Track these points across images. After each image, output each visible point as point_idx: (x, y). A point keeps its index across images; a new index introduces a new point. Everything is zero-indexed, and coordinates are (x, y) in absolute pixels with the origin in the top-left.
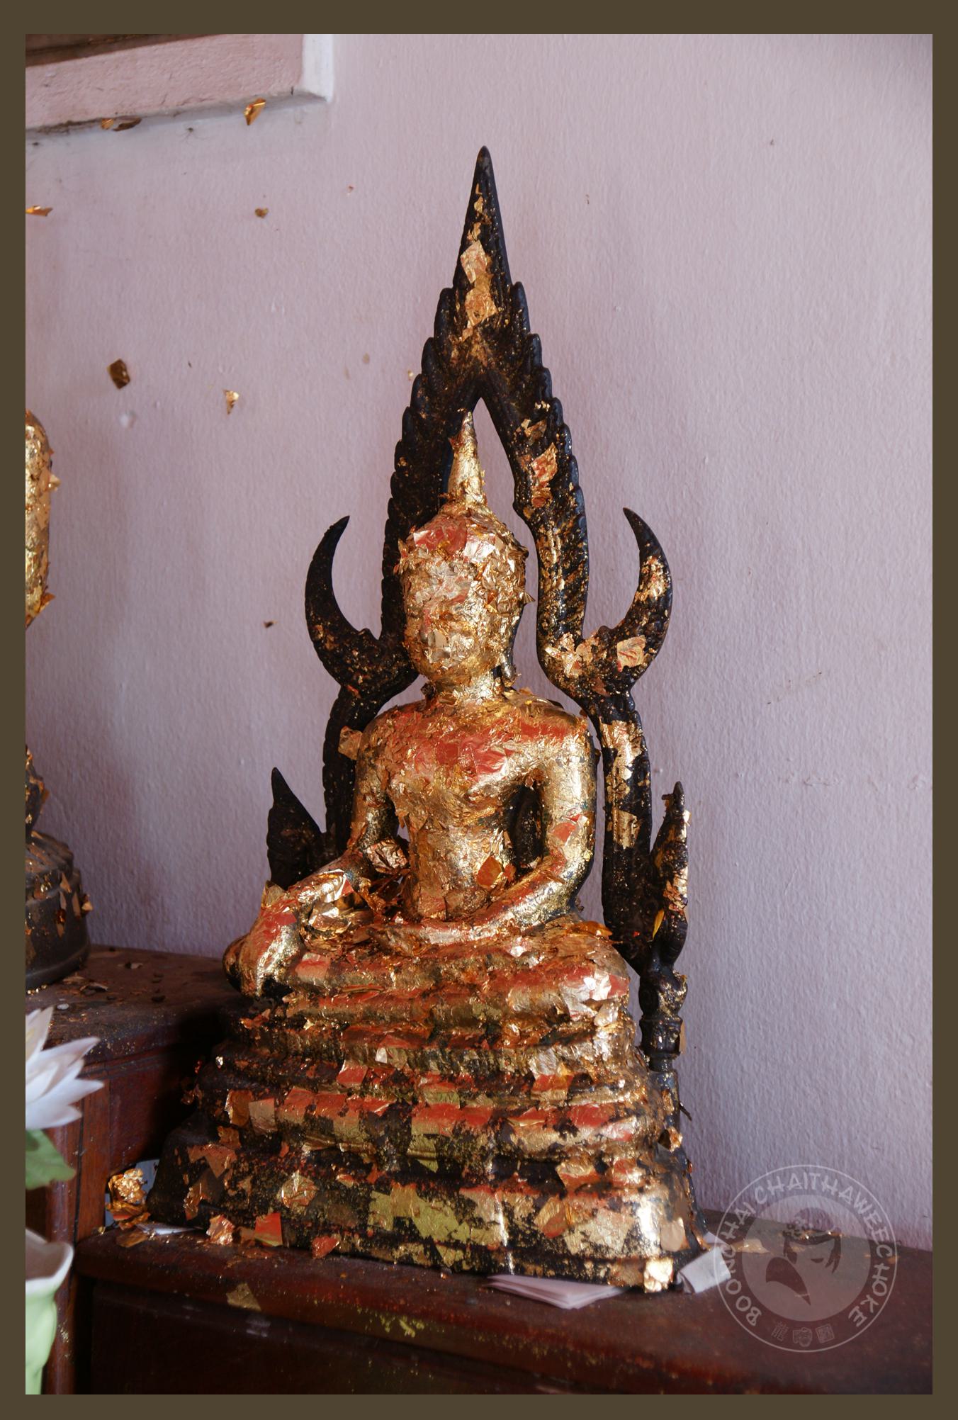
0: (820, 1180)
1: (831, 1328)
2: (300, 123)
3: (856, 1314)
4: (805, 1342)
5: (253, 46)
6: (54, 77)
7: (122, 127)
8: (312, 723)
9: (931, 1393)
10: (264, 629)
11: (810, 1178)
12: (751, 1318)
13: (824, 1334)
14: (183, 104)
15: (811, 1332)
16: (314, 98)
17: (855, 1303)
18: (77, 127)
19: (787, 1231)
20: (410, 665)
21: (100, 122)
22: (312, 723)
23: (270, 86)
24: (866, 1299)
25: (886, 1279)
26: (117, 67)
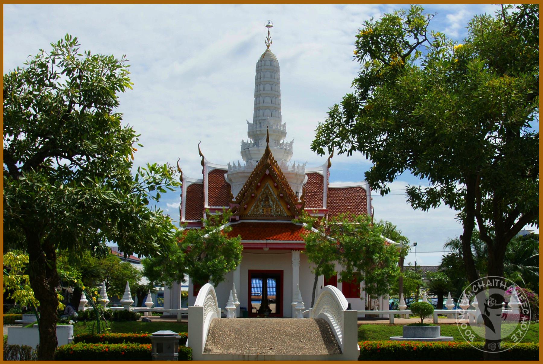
0: (499, 283)
3: (514, 337)
4: (493, 349)
9: (538, 360)
11: (495, 282)
12: (471, 339)
17: (514, 332)
20: (183, 341)
25: (526, 323)
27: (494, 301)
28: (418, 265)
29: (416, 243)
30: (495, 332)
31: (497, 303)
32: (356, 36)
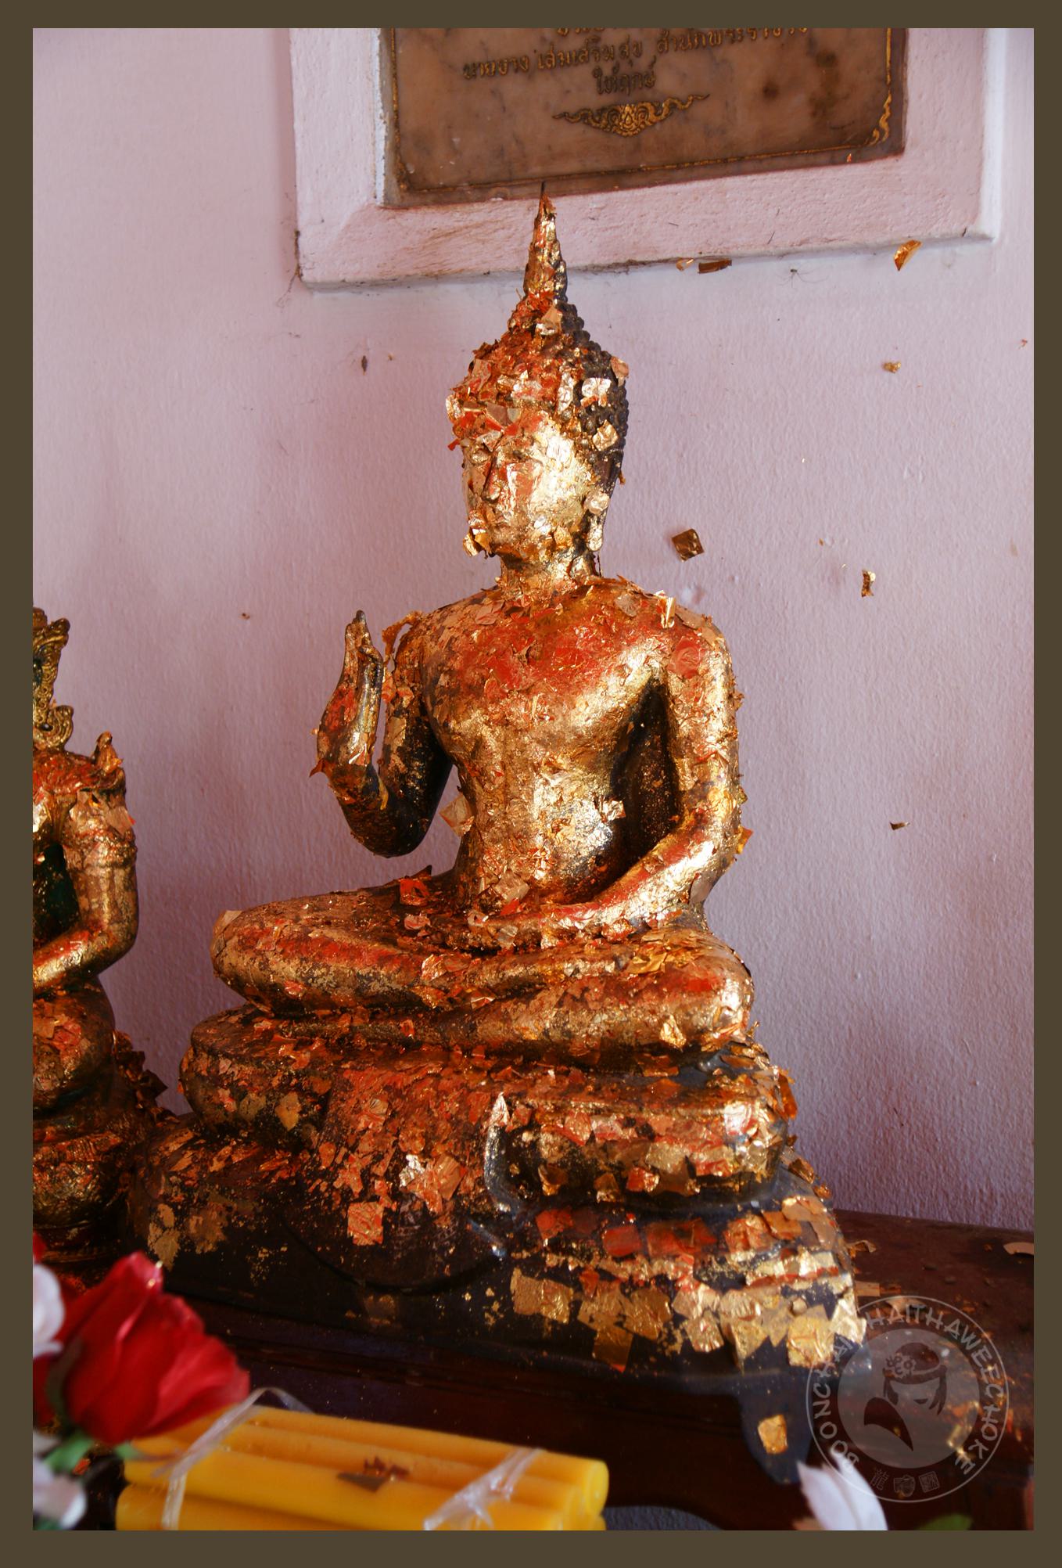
1: (935, 1476)
2: (949, 266)
5: (900, 180)
6: (601, 209)
7: (704, 268)
8: (960, 933)
10: (891, 831)
13: (928, 1481)
14: (800, 245)
15: (913, 1480)
16: (984, 238)
18: (644, 268)
19: (887, 1368)
21: (677, 262)
22: (960, 933)
23: (932, 226)
24: (975, 1443)
26: (696, 199)
27: (909, 1362)
28: (681, 1293)
29: (676, 540)
30: (911, 1447)
31: (917, 1368)
32: (899, 269)
